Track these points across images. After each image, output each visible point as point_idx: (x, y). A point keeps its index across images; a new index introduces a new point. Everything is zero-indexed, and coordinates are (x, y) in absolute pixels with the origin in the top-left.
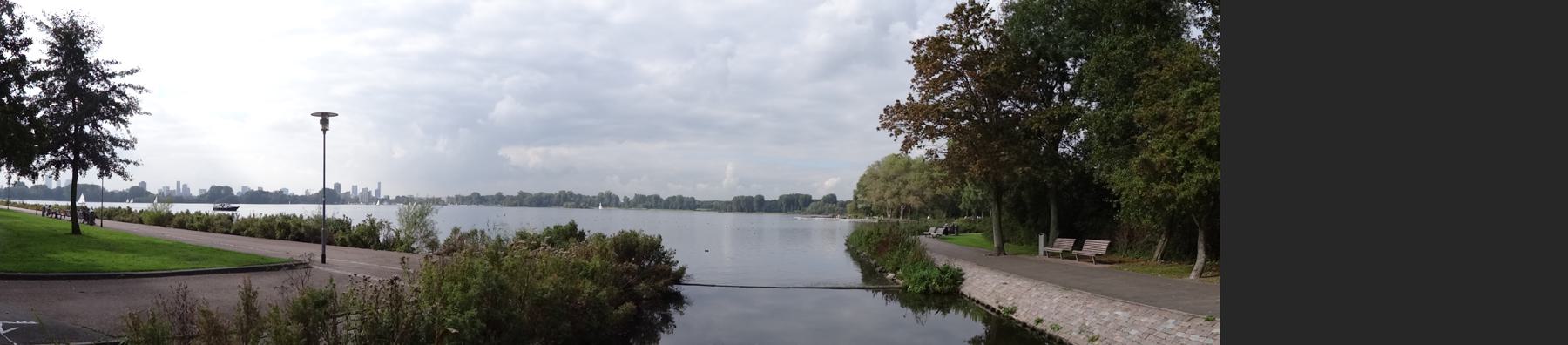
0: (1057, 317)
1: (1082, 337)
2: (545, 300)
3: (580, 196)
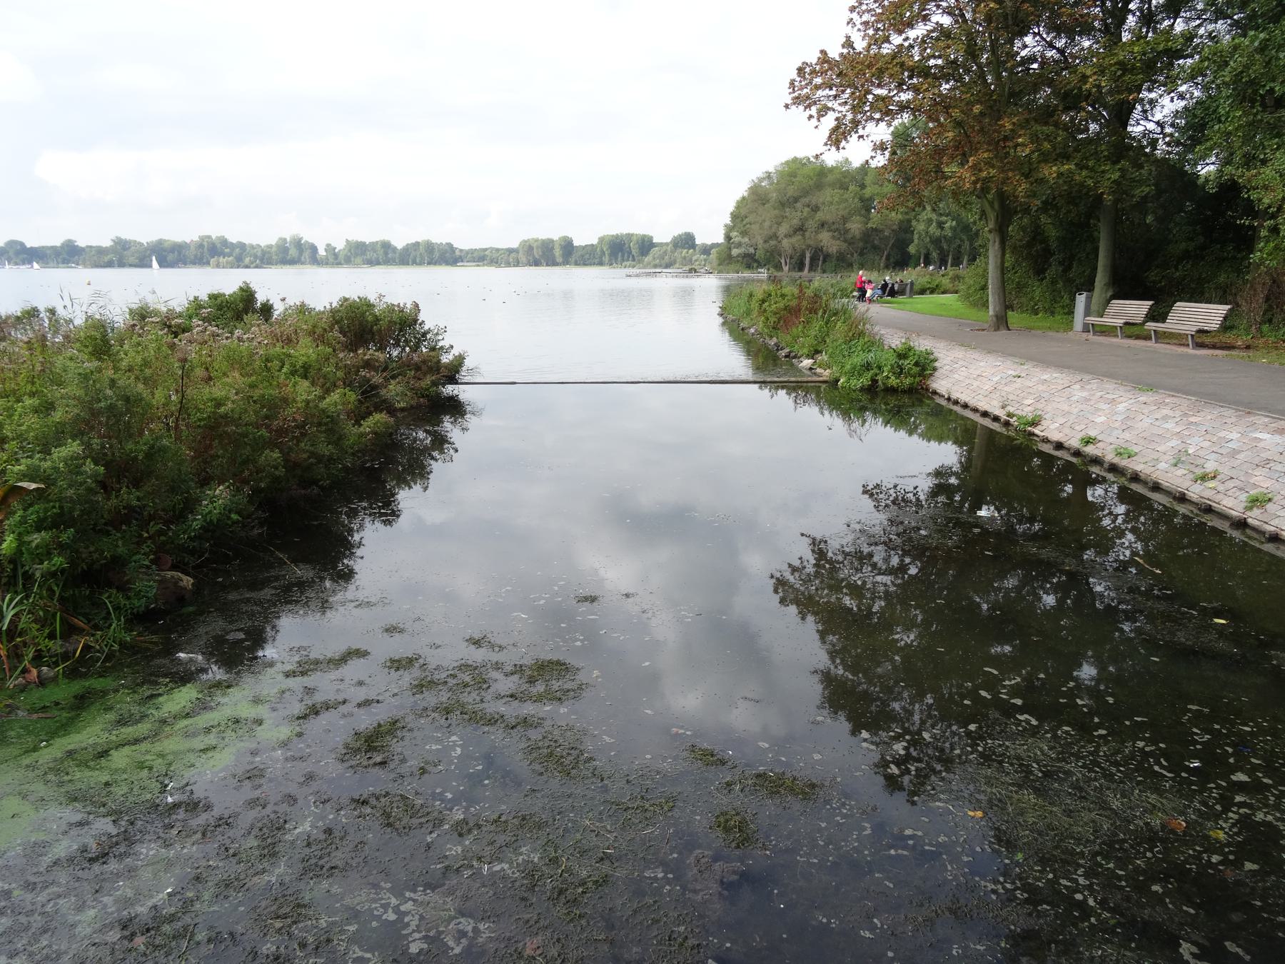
0: (1127, 436)
1: (1180, 472)
2: (225, 416)
3: (242, 246)
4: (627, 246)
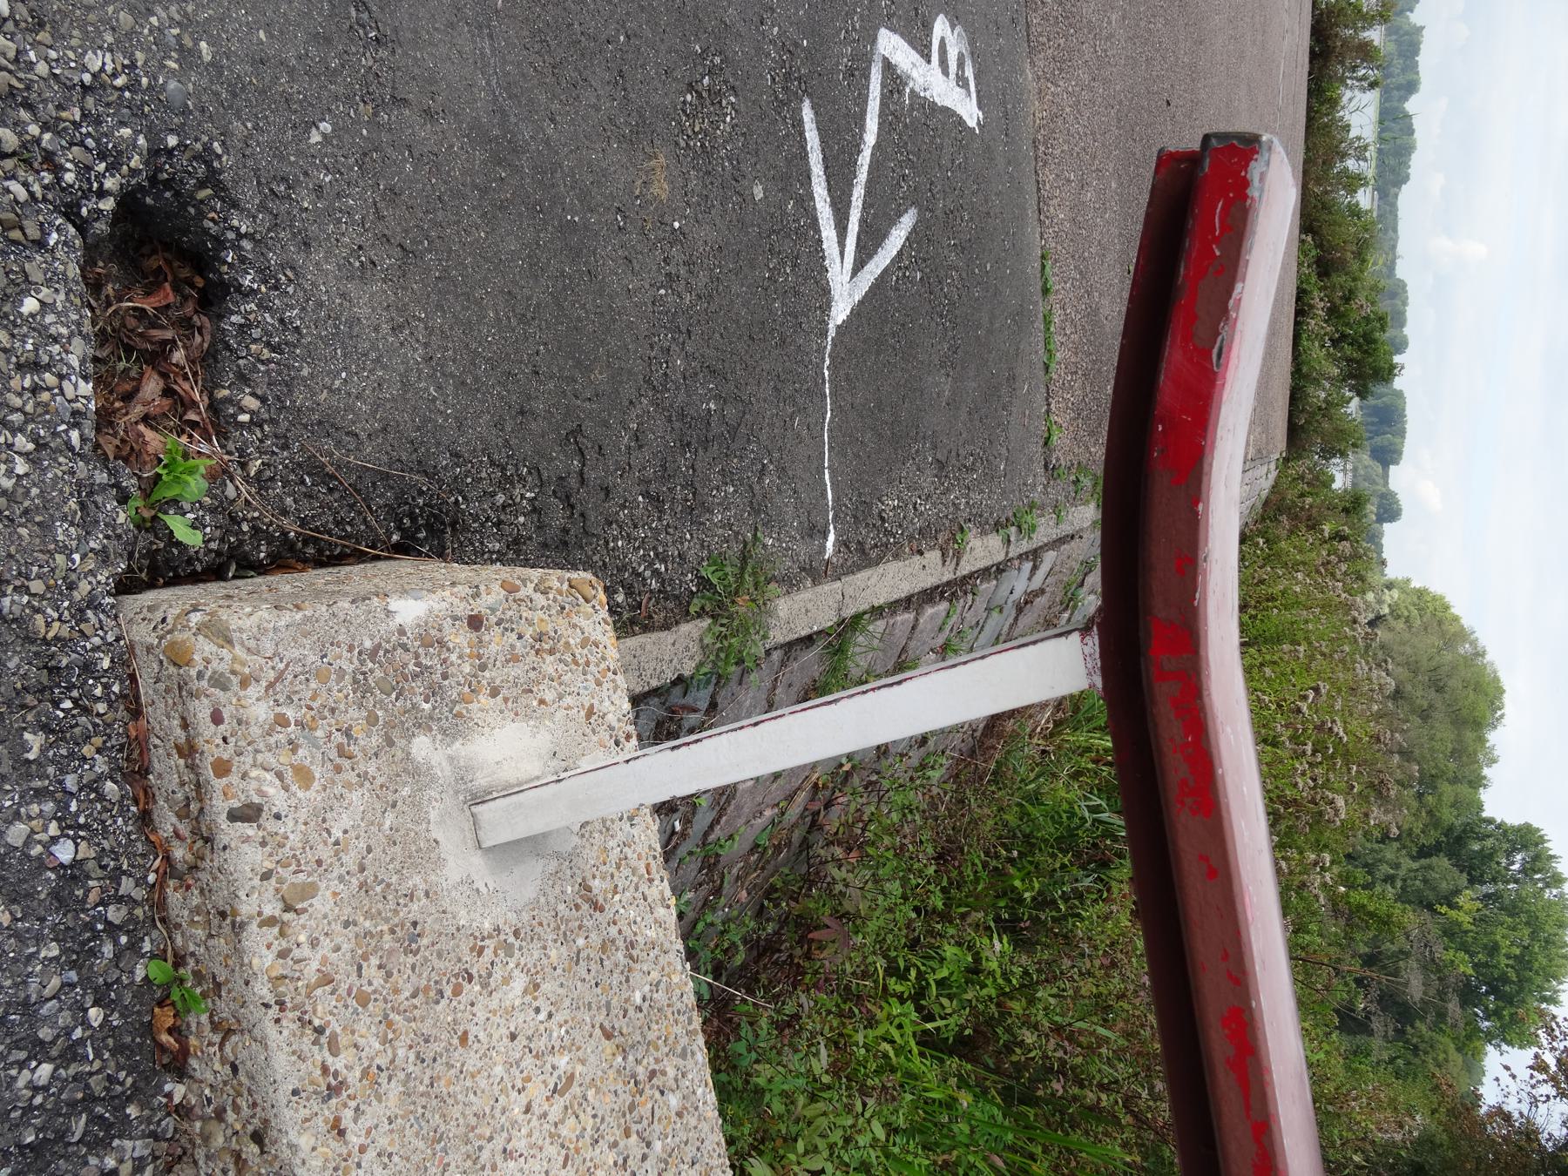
4: (1388, 429)
